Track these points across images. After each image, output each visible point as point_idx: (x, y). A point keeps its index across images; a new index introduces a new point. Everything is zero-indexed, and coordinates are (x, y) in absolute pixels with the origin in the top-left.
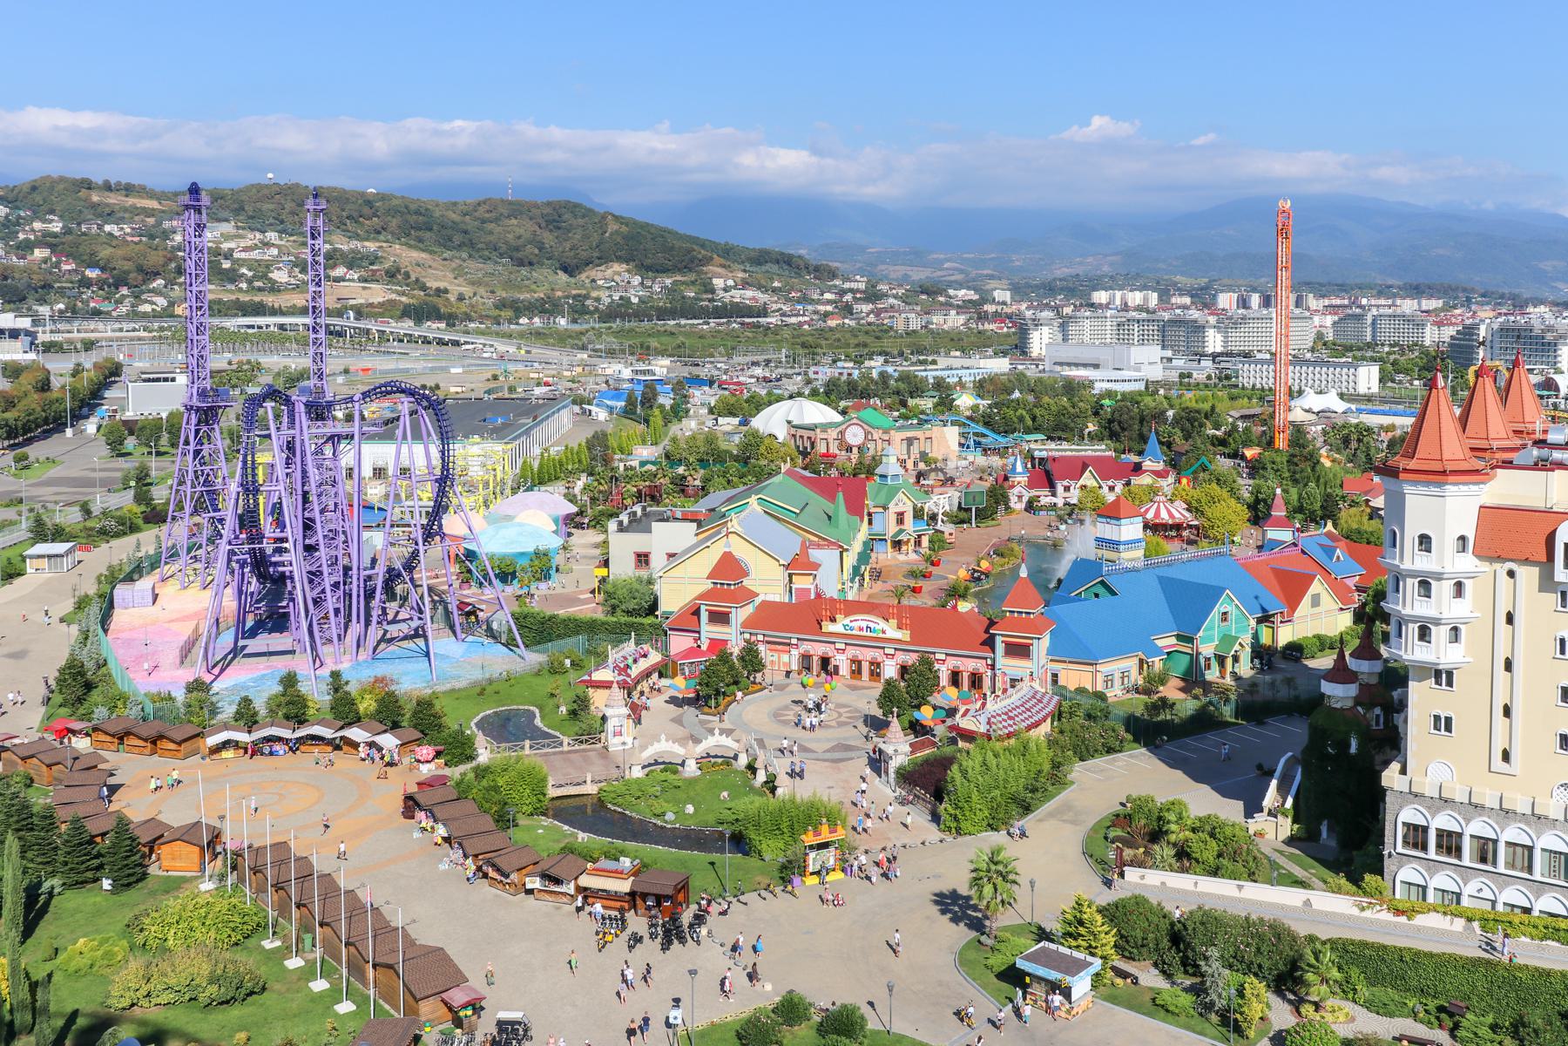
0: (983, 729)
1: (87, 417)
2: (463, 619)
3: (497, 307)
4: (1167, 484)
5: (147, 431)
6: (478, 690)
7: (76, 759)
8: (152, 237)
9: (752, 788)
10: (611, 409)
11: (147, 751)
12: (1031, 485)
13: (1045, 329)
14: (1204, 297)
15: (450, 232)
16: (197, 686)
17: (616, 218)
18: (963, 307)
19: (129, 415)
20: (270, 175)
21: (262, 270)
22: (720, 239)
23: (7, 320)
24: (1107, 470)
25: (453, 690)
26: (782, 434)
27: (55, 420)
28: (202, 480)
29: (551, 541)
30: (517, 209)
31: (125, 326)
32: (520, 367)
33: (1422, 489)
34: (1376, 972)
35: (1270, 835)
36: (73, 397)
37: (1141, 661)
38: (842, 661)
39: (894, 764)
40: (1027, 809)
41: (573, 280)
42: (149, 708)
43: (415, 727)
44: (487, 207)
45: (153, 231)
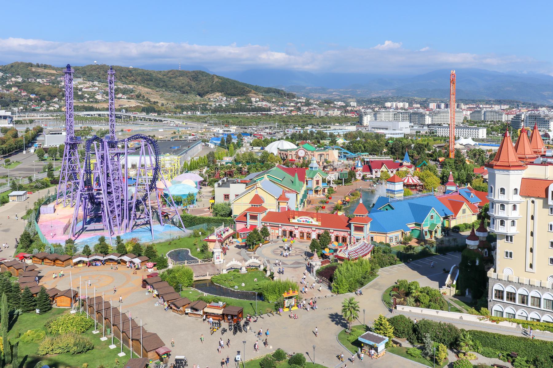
0: (347, 256)
1: (31, 147)
2: (163, 218)
3: (175, 108)
4: (412, 170)
5: (52, 152)
6: (169, 243)
7: (27, 267)
8: (54, 83)
9: (265, 277)
10: (215, 144)
11: (52, 264)
12: (364, 171)
13: (369, 116)
14: (424, 105)
15: (159, 82)
16: (69, 241)
17: (217, 77)
18: (340, 108)
19: (46, 146)
20: (95, 62)
21: (93, 95)
22: (254, 84)
23: (2, 113)
24: (391, 165)
25: (160, 243)
26: (276, 153)
27: (19, 148)
28: (71, 169)
29: (194, 190)
30: (182, 74)
31: (44, 115)
32: (183, 129)
33: (502, 172)
34: (485, 342)
35: (448, 294)
36: (26, 140)
37: (402, 233)
38: (297, 233)
39: (315, 269)
40: (362, 285)
41: (202, 99)
42: (53, 249)
43: (146, 256)
44: (172, 73)
45: (54, 81)
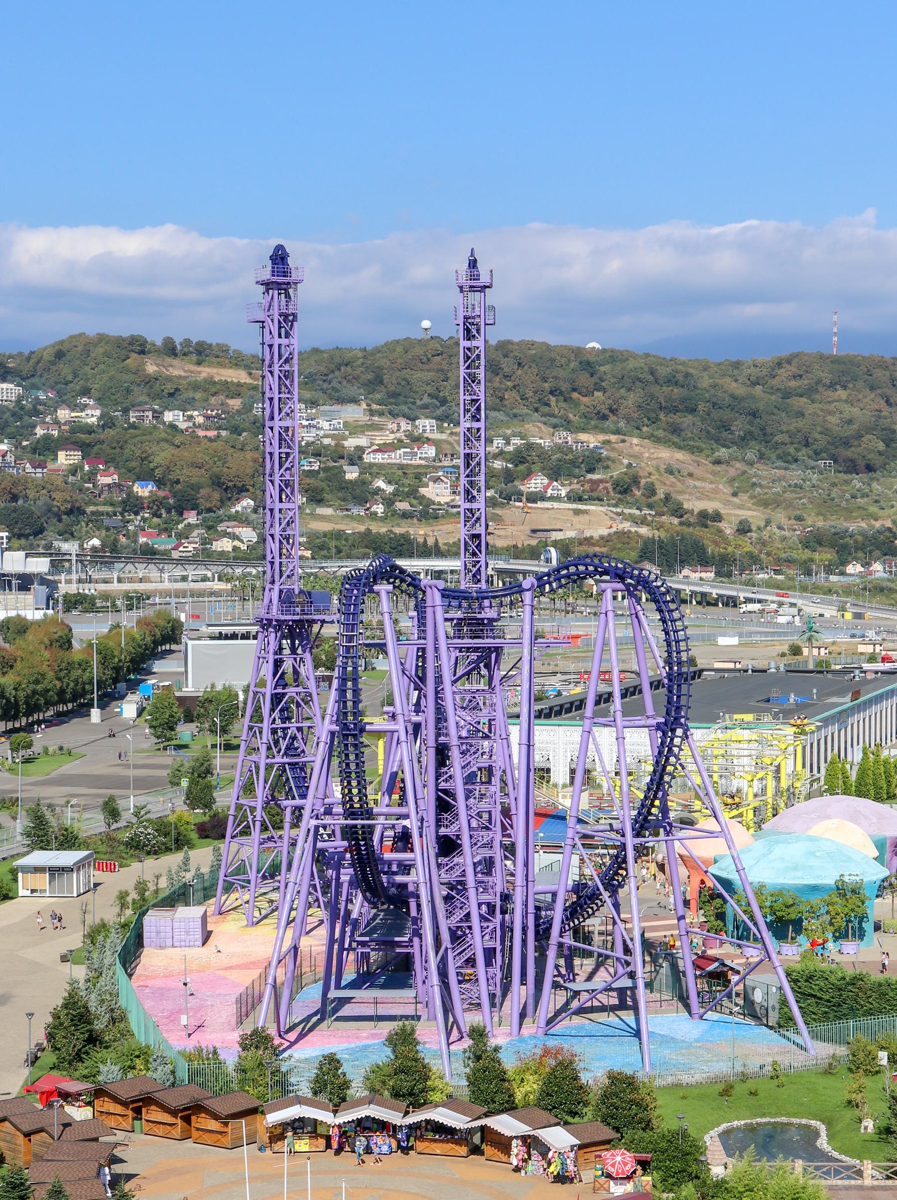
1: (122, 697)
2: (703, 985)
3: (806, 545)
5: (213, 711)
6: (720, 1087)
7: (66, 1125)
8: (236, 430)
11: (177, 1132)
15: (727, 414)
19: (190, 689)
20: (426, 324)
21: (409, 481)
23: (15, 562)
25: (678, 1086)
27: (75, 697)
28: (283, 745)
30: (847, 371)
31: (191, 572)
36: (104, 661)
42: (183, 1074)
44: (793, 369)
